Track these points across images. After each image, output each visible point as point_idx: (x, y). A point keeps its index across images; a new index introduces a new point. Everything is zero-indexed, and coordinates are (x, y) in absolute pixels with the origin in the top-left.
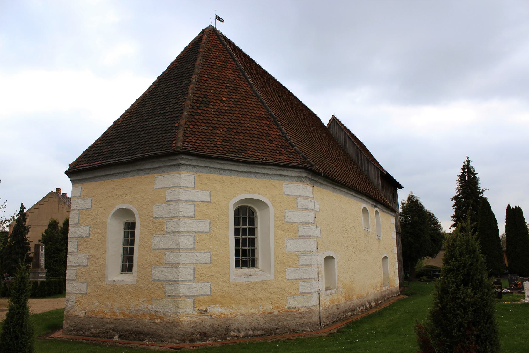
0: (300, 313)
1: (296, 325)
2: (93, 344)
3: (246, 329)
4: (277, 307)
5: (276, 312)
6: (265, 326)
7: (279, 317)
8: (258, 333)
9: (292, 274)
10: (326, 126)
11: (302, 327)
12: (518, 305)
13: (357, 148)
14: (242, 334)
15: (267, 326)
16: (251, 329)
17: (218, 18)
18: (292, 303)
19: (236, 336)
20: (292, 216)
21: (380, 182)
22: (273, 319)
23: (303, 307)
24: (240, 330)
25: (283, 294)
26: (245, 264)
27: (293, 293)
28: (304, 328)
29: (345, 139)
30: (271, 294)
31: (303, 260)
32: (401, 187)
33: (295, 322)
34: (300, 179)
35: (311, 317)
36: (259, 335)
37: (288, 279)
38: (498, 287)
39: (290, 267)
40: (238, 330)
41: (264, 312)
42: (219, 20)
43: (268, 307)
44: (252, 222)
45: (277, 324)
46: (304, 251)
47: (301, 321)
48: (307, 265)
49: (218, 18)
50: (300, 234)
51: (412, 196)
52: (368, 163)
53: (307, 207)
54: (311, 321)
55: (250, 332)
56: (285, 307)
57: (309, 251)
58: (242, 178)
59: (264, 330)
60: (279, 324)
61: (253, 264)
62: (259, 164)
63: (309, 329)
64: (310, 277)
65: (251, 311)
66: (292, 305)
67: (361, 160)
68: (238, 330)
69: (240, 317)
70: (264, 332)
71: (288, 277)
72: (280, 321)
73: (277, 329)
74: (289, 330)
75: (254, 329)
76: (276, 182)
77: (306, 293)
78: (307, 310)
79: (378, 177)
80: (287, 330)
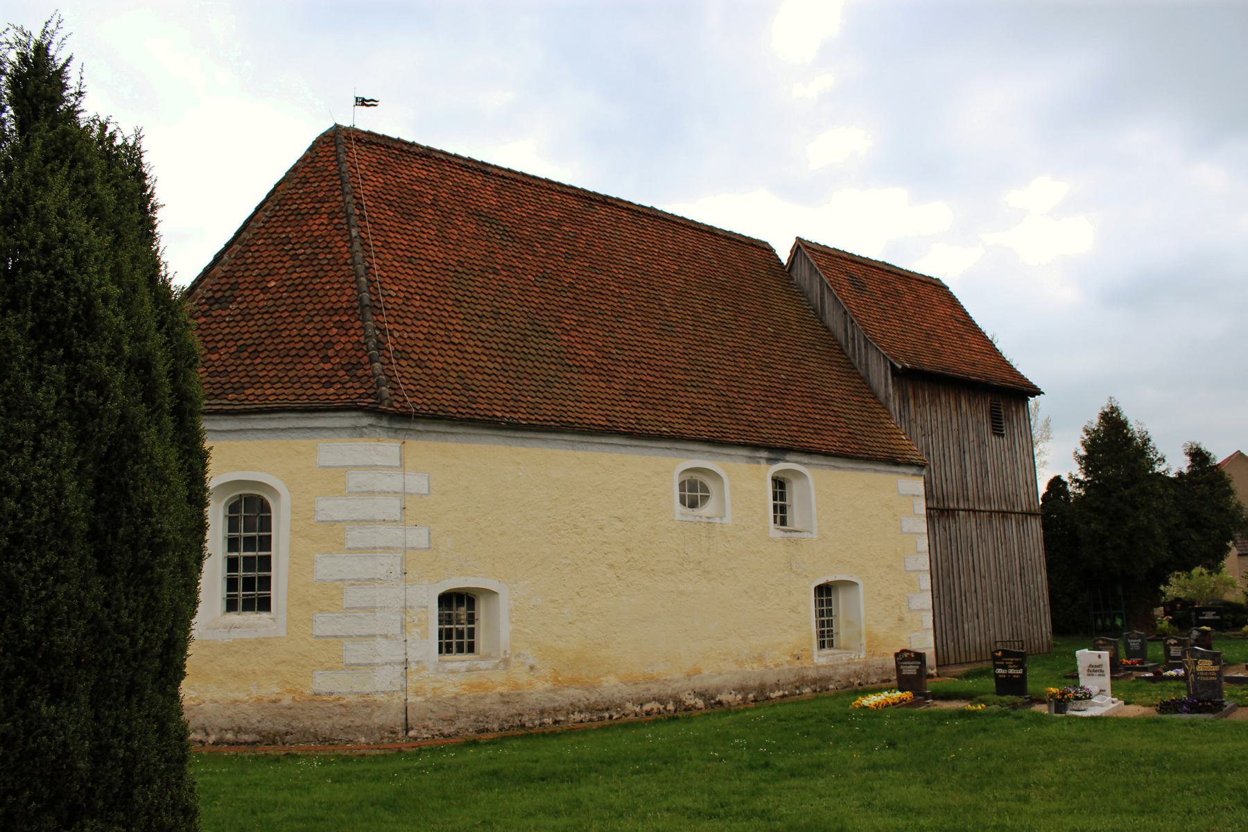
0: (342, 705)
1: (333, 728)
2: (637, 761)
3: (221, 730)
4: (290, 691)
5: (287, 700)
6: (261, 725)
7: (293, 711)
8: (246, 737)
9: (325, 625)
10: (785, 261)
11: (348, 733)
12: (1082, 718)
13: (845, 313)
14: (212, 738)
15: (267, 726)
16: (232, 729)
17: (362, 102)
18: (323, 683)
19: (201, 742)
20: (331, 508)
21: (891, 391)
22: (281, 715)
23: (350, 693)
24: (209, 730)
25: (304, 666)
26: (249, 606)
27: (327, 665)
28: (351, 737)
29: (822, 293)
30: (277, 664)
31: (354, 597)
32: (1036, 392)
33: (330, 722)
34: (356, 431)
35: (370, 716)
36: (246, 743)
37: (317, 637)
38: (1015, 663)
39: (321, 611)
40: (205, 730)
41: (259, 700)
42: (363, 104)
43: (271, 689)
44: (266, 524)
45: (289, 725)
46: (358, 580)
47: (345, 721)
48: (363, 608)
49: (362, 102)
50: (350, 544)
51: (1114, 409)
52: (866, 347)
53: (370, 488)
54: (369, 723)
55: (230, 736)
56: (308, 692)
57: (369, 580)
58: (226, 442)
59: (259, 733)
60: (294, 724)
61: (264, 605)
62: (260, 411)
63: (363, 739)
64: (371, 632)
65: (232, 696)
66: (324, 689)
67: (853, 339)
68: (205, 730)
69: (208, 707)
70: (258, 738)
71: (317, 632)
72: (295, 718)
73: (287, 733)
74: (316, 737)
75: (239, 730)
76: (302, 443)
77: (359, 665)
78: (361, 700)
79: (886, 379)
80: (311, 738)
